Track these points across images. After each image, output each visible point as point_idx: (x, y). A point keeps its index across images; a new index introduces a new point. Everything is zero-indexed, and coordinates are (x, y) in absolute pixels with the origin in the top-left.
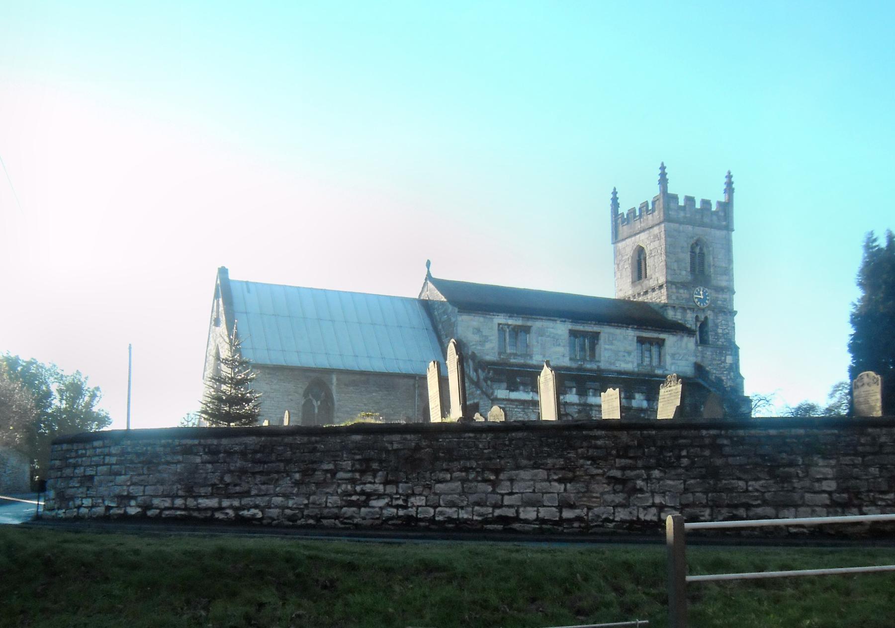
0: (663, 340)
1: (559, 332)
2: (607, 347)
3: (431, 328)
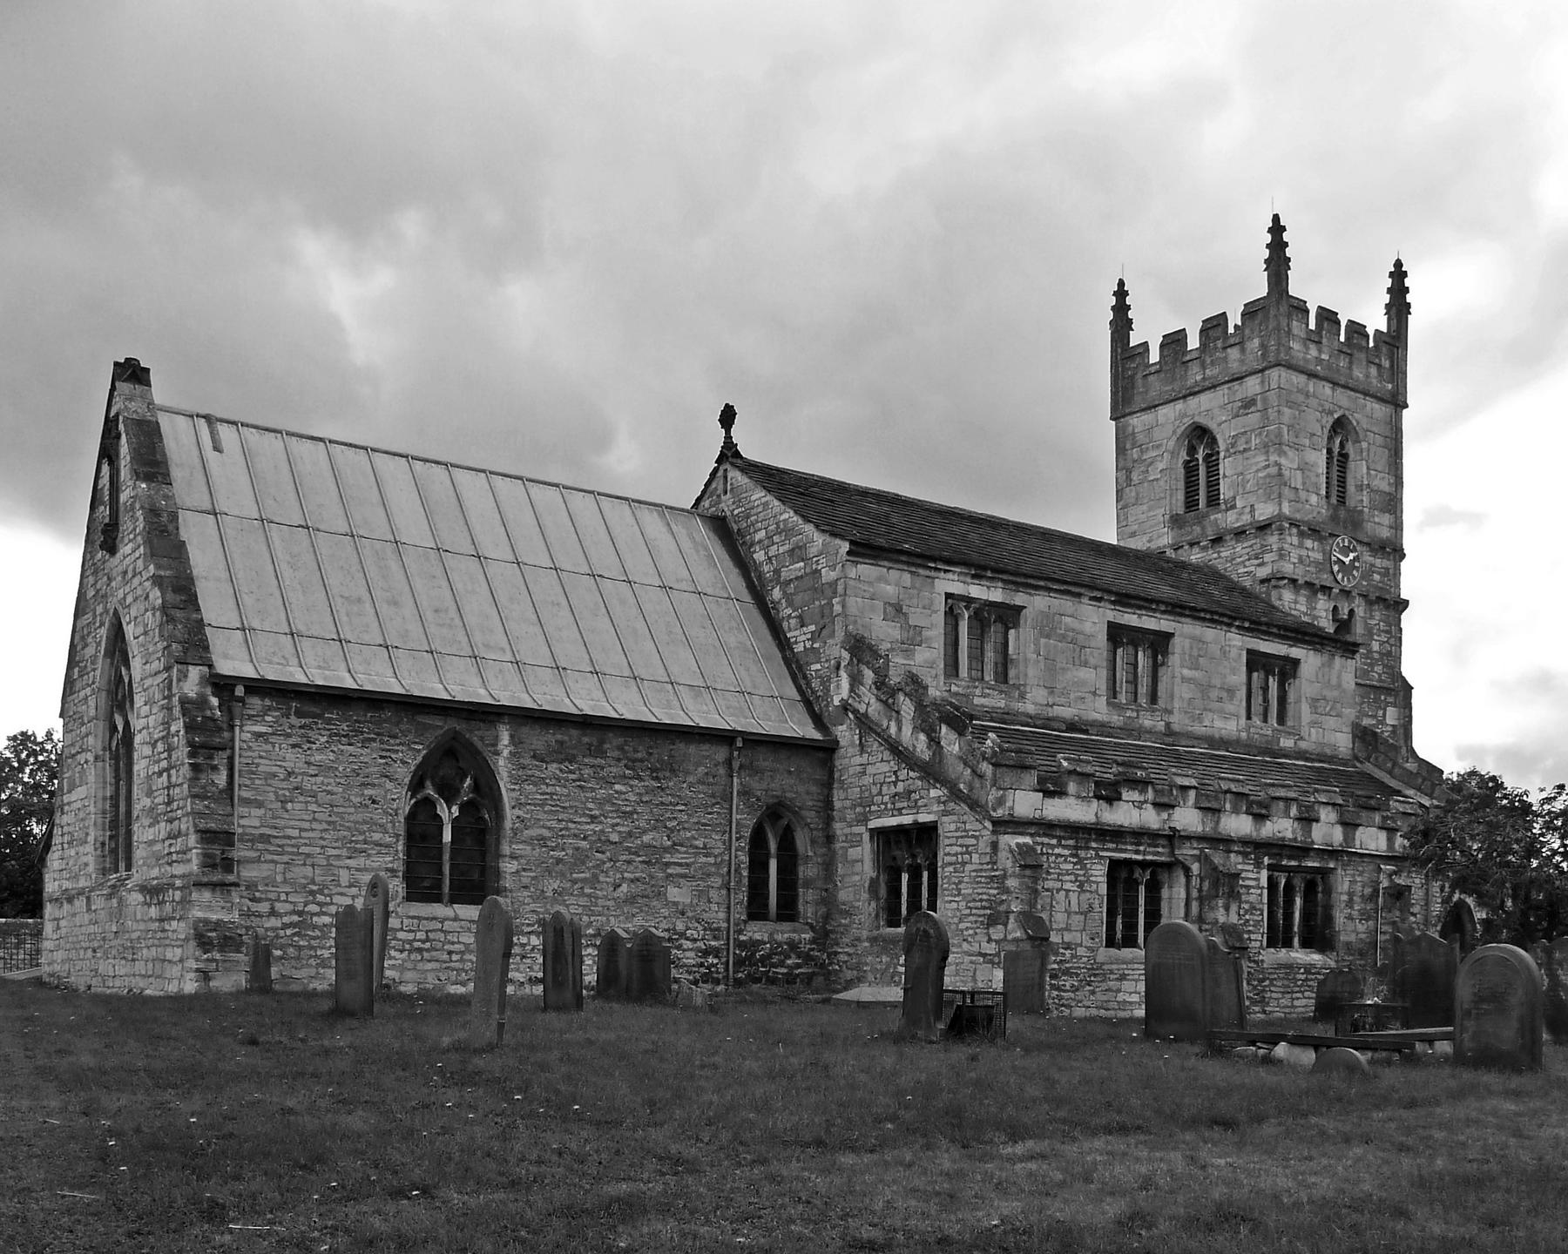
0: (1296, 663)
1: (1088, 627)
2: (1186, 672)
3: (747, 598)
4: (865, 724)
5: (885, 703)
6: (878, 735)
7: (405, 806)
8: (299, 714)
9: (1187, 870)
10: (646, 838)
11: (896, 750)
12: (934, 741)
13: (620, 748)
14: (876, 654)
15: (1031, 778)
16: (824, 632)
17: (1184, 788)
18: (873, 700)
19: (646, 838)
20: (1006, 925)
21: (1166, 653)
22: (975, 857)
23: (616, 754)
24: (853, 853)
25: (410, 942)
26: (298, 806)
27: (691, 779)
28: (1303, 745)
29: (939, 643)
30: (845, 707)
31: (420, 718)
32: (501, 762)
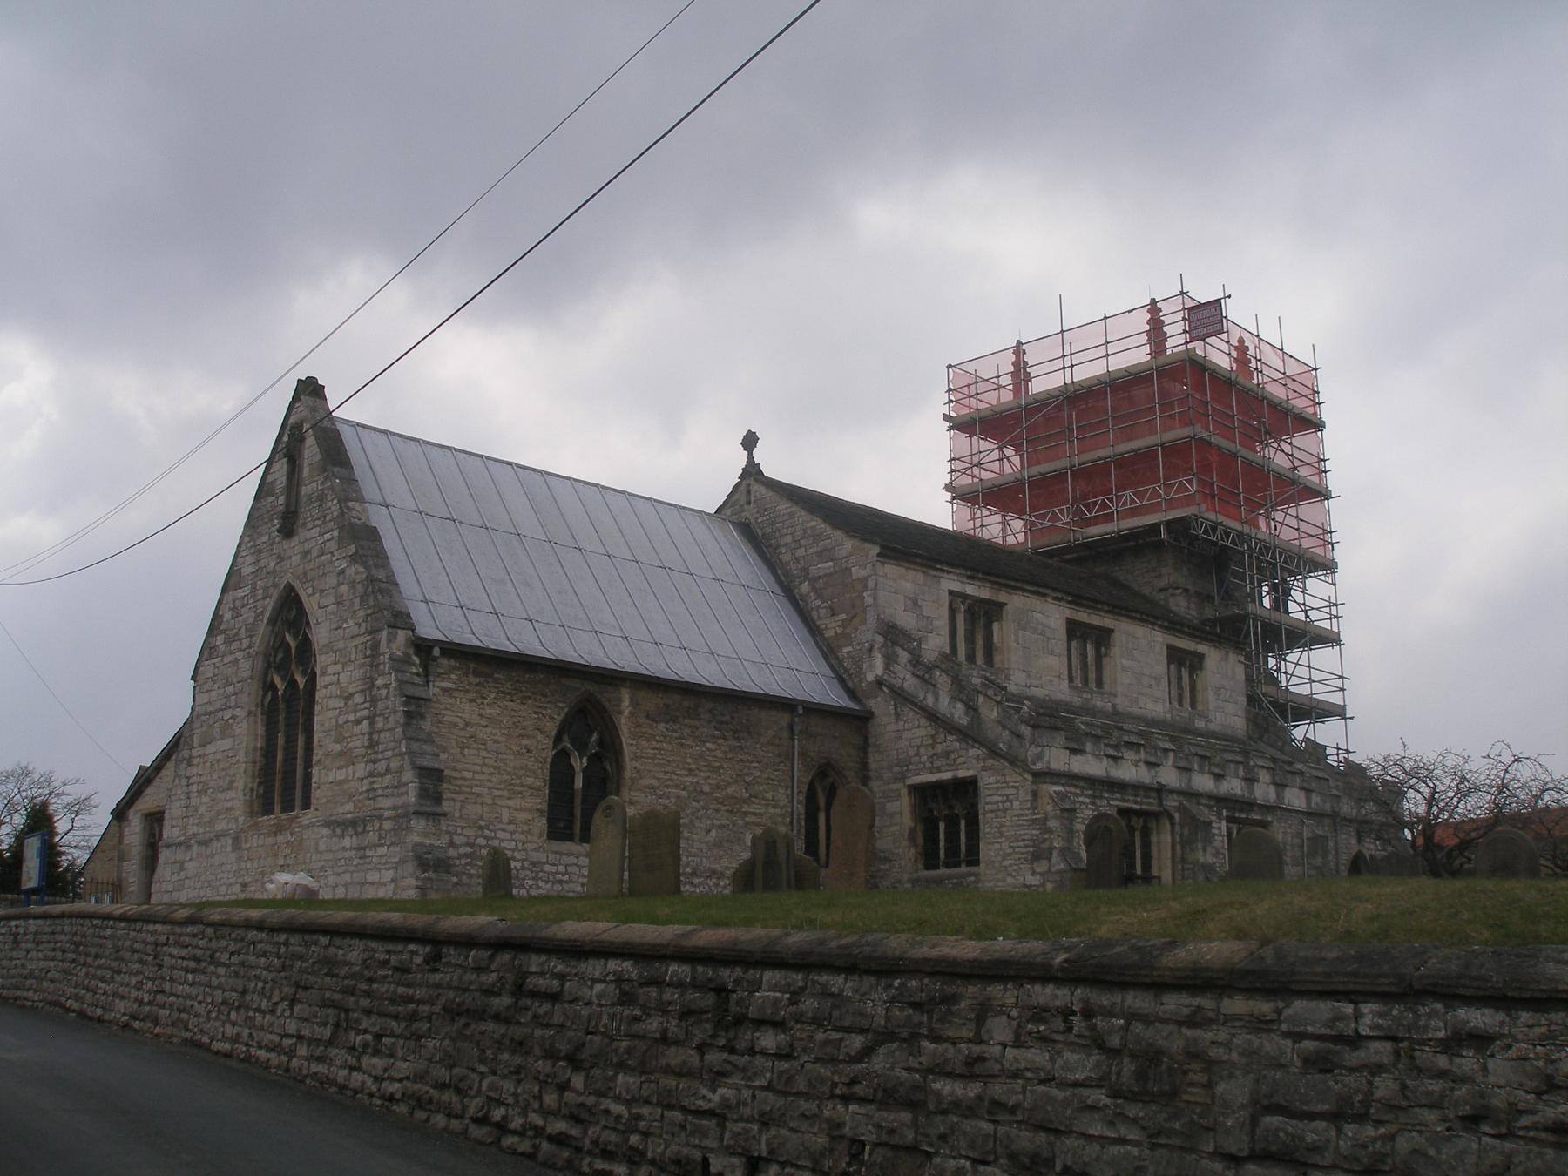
3: (778, 591)
4: (901, 696)
5: (922, 678)
6: (915, 705)
7: (549, 754)
8: (476, 674)
9: (1171, 818)
10: (730, 790)
11: (933, 717)
12: (971, 708)
13: (710, 711)
14: (910, 638)
15: (1061, 739)
16: (856, 621)
17: (1166, 750)
18: (908, 676)
19: (730, 790)
20: (1049, 859)
21: (1108, 646)
22: (1016, 804)
23: (707, 716)
24: (892, 807)
25: (554, 874)
26: (473, 752)
27: (763, 740)
28: (1212, 727)
29: (945, 631)
30: (880, 683)
31: (564, 681)
32: (623, 721)
